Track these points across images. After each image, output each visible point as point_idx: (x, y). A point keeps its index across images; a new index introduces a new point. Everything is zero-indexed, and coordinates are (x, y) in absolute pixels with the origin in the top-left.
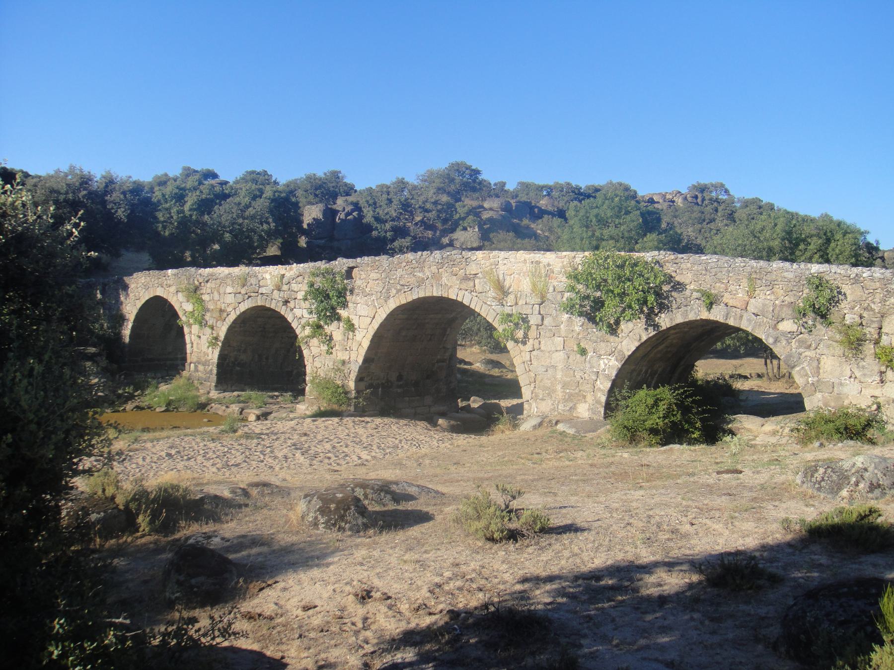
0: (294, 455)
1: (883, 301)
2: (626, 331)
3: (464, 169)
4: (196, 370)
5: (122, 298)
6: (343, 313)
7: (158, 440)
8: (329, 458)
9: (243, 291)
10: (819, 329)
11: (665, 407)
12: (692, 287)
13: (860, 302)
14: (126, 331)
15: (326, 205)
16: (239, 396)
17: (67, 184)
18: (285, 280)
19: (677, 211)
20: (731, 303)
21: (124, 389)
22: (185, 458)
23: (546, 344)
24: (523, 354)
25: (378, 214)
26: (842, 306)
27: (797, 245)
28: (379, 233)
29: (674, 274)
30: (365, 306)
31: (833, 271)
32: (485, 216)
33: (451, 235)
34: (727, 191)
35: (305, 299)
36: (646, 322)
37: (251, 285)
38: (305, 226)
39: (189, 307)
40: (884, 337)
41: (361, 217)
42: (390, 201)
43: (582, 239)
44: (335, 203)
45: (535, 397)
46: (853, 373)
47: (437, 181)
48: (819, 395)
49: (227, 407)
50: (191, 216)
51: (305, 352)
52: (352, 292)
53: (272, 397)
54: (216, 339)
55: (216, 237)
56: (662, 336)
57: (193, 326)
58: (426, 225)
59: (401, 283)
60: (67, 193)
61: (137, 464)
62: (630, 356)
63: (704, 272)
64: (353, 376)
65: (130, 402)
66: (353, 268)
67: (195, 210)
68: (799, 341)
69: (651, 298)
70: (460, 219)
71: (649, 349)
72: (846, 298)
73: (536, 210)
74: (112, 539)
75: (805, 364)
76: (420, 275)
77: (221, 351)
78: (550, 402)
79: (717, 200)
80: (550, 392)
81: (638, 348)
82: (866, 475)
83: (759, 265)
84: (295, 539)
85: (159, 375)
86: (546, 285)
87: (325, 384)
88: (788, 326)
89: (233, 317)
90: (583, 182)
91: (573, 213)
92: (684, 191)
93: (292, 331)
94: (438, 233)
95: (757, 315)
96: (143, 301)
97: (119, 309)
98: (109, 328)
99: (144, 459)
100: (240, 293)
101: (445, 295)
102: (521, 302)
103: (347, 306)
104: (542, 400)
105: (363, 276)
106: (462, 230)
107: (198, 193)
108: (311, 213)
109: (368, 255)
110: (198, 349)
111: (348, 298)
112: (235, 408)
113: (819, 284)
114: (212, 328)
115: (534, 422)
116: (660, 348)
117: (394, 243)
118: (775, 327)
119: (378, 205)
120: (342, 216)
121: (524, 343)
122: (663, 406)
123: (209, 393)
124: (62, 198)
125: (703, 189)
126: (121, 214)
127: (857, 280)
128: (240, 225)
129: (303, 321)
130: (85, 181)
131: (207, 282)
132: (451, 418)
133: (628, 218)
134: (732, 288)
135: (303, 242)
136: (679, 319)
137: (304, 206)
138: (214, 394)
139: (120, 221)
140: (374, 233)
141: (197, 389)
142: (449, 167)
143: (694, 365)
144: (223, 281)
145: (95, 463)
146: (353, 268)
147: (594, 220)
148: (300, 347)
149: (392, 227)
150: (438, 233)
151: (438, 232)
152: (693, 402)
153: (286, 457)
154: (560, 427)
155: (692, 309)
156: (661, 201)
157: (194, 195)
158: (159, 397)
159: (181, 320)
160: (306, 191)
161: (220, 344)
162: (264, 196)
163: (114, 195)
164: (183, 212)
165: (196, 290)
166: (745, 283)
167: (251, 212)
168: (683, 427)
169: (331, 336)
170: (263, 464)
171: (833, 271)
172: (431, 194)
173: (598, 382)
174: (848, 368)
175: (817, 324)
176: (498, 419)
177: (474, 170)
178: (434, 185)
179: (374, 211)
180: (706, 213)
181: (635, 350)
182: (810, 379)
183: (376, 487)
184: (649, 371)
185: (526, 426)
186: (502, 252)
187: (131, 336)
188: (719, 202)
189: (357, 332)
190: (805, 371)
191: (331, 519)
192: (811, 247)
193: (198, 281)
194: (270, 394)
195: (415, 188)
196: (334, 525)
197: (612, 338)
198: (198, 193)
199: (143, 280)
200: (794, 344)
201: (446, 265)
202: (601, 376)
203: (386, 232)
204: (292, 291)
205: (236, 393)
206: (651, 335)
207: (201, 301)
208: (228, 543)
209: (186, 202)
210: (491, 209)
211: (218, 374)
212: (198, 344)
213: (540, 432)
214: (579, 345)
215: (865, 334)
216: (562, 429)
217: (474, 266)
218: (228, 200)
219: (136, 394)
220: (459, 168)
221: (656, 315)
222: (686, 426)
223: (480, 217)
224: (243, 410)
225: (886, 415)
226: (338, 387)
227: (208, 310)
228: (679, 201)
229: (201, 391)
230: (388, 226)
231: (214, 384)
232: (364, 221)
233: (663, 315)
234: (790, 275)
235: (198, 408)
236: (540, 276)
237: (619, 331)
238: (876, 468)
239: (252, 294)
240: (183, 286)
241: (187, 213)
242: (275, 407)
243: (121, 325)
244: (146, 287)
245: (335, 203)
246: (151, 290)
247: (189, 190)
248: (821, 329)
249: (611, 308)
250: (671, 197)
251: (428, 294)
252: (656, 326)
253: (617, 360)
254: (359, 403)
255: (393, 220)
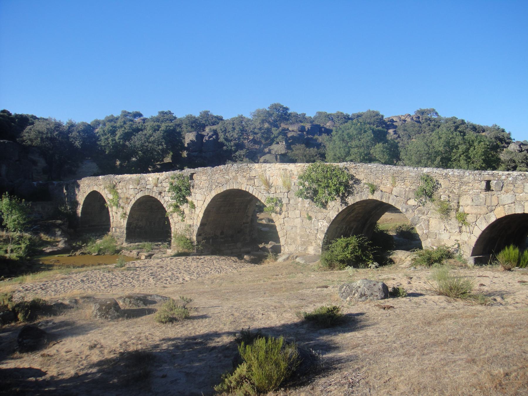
0: (149, 279)
1: (459, 188)
2: (331, 206)
3: (279, 108)
4: (116, 231)
5: (77, 192)
6: (189, 198)
7: (80, 272)
8: (167, 280)
9: (138, 188)
10: (428, 204)
11: (351, 248)
12: (364, 182)
13: (448, 188)
14: (79, 210)
15: (198, 133)
16: (138, 245)
17: (47, 129)
18: (159, 181)
19: (406, 126)
20: (384, 190)
21: (76, 243)
22: (91, 282)
23: (291, 214)
24: (280, 219)
25: (227, 136)
26: (439, 191)
27: (452, 149)
28: (228, 147)
29: (355, 175)
30: (200, 195)
31: (434, 172)
32: (290, 135)
33: (269, 147)
34: (436, 113)
35: (169, 192)
36: (341, 201)
37: (142, 184)
38: (186, 145)
39: (111, 197)
40: (461, 208)
41: (217, 138)
42: (234, 129)
43: (340, 148)
44: (204, 131)
45: (287, 243)
46: (446, 227)
47: (262, 116)
48: (429, 240)
49: (131, 252)
50: (120, 142)
51: (171, 221)
52: (193, 187)
53: (157, 245)
54: (125, 214)
55: (133, 153)
56: (350, 210)
57: (113, 207)
58: (254, 141)
59: (218, 182)
60: (47, 133)
61: (64, 286)
62: (333, 220)
63: (370, 173)
64: (195, 233)
65: (79, 250)
66: (193, 174)
67: (122, 139)
68: (419, 210)
69: (342, 188)
70: (275, 137)
71: (345, 216)
72: (441, 186)
73: (323, 129)
74: (6, 324)
75: (422, 223)
76: (227, 177)
77: (128, 221)
78: (294, 246)
79: (430, 119)
80: (294, 240)
81: (337, 216)
82: (359, 289)
83: (397, 169)
84: (84, 322)
85: (98, 234)
86: (290, 182)
87: (181, 238)
88: (412, 202)
89: (133, 202)
90: (350, 112)
91: (335, 133)
92: (412, 114)
93: (164, 208)
94: (262, 146)
95: (397, 196)
96: (87, 194)
97: (75, 198)
98: (69, 209)
99: (68, 283)
100: (136, 188)
101: (240, 188)
102: (278, 191)
103: (191, 195)
104: (291, 244)
105: (199, 178)
106: (276, 144)
107: (123, 129)
108: (189, 137)
109: (201, 167)
110: (116, 220)
111: (191, 190)
112: (135, 252)
113: (427, 179)
114: (123, 208)
115: (284, 257)
116: (352, 215)
117: (236, 153)
118: (406, 203)
119: (227, 131)
120: (207, 138)
121: (280, 214)
122: (350, 247)
123: (122, 244)
124: (44, 136)
125: (423, 112)
126: (77, 144)
127: (446, 176)
128: (146, 146)
129: (169, 203)
130: (58, 126)
131: (120, 182)
132: (253, 255)
133: (366, 135)
134: (384, 182)
135: (185, 154)
136: (358, 200)
137: (185, 133)
138: (125, 245)
139: (77, 148)
140: (225, 148)
141: (116, 242)
142: (271, 106)
143: (376, 223)
144: (128, 182)
145: (42, 286)
146: (193, 174)
147: (346, 136)
148: (168, 218)
149: (235, 144)
150: (262, 146)
151: (262, 145)
152: (368, 244)
153: (144, 280)
154: (298, 260)
155: (364, 194)
156: (398, 121)
157: (121, 130)
158: (95, 247)
159: (107, 204)
160: (187, 125)
161: (127, 217)
162: (160, 129)
163: (73, 133)
164: (115, 140)
165: (114, 187)
166: (390, 179)
167: (152, 139)
168: (362, 258)
169: (183, 212)
170: (130, 284)
171: (434, 172)
172: (258, 124)
173: (318, 235)
174: (443, 224)
175: (427, 201)
176: (267, 256)
177: (285, 108)
178: (260, 118)
179: (225, 135)
180: (422, 127)
181: (336, 217)
182: (424, 231)
183: (136, 298)
184: (348, 227)
185: (280, 259)
186: (268, 164)
187: (81, 213)
188: (431, 121)
189: (196, 209)
190: (422, 227)
191: (102, 313)
192: (460, 150)
193: (115, 182)
194: (156, 243)
195: (249, 120)
196: (103, 316)
197: (324, 210)
198: (123, 129)
199: (87, 182)
200: (416, 212)
201: (240, 172)
202: (319, 232)
203: (231, 147)
204: (163, 187)
205: (137, 244)
206: (344, 208)
207: (116, 193)
208: (55, 325)
209: (116, 134)
210: (293, 131)
211: (127, 234)
212: (116, 217)
213: (285, 263)
214: (308, 214)
215: (451, 206)
216: (298, 261)
217: (254, 172)
218: (139, 133)
219: (83, 245)
220: (276, 107)
221: (346, 197)
222: (364, 258)
223: (287, 136)
224: (139, 253)
225: (463, 250)
226: (188, 239)
227: (120, 198)
228: (408, 120)
229: (119, 243)
230: (232, 143)
231: (125, 239)
232: (219, 141)
233: (350, 197)
234: (413, 174)
235: (115, 253)
236: (287, 176)
237: (328, 206)
238: (364, 286)
239: (143, 189)
240: (107, 185)
241: (118, 141)
242: (157, 251)
243: (76, 207)
244: (89, 186)
245: (204, 131)
246: (91, 187)
247: (119, 127)
248: (429, 204)
249: (323, 195)
250: (404, 118)
251: (231, 188)
252: (346, 203)
253: (327, 222)
254: (199, 248)
255: (235, 140)
